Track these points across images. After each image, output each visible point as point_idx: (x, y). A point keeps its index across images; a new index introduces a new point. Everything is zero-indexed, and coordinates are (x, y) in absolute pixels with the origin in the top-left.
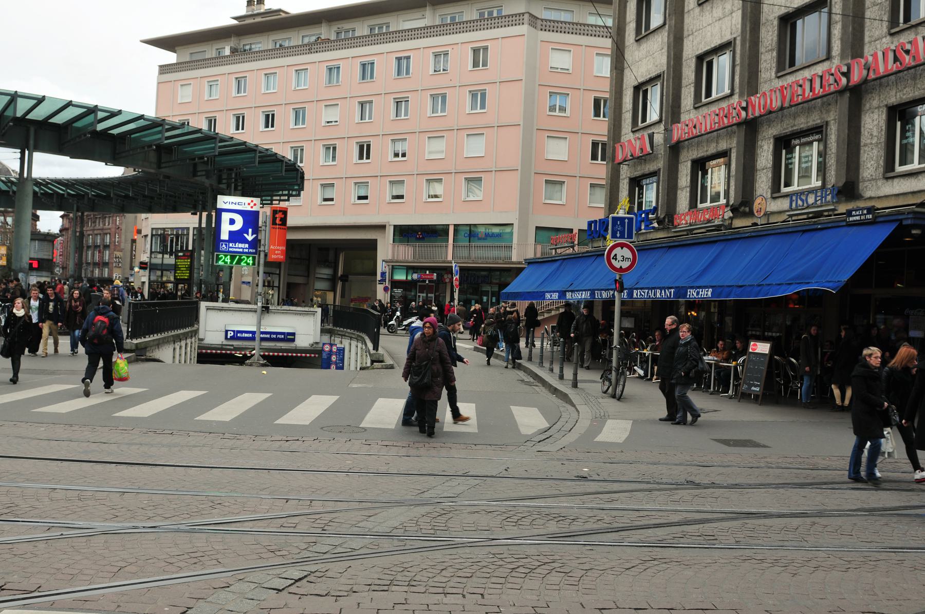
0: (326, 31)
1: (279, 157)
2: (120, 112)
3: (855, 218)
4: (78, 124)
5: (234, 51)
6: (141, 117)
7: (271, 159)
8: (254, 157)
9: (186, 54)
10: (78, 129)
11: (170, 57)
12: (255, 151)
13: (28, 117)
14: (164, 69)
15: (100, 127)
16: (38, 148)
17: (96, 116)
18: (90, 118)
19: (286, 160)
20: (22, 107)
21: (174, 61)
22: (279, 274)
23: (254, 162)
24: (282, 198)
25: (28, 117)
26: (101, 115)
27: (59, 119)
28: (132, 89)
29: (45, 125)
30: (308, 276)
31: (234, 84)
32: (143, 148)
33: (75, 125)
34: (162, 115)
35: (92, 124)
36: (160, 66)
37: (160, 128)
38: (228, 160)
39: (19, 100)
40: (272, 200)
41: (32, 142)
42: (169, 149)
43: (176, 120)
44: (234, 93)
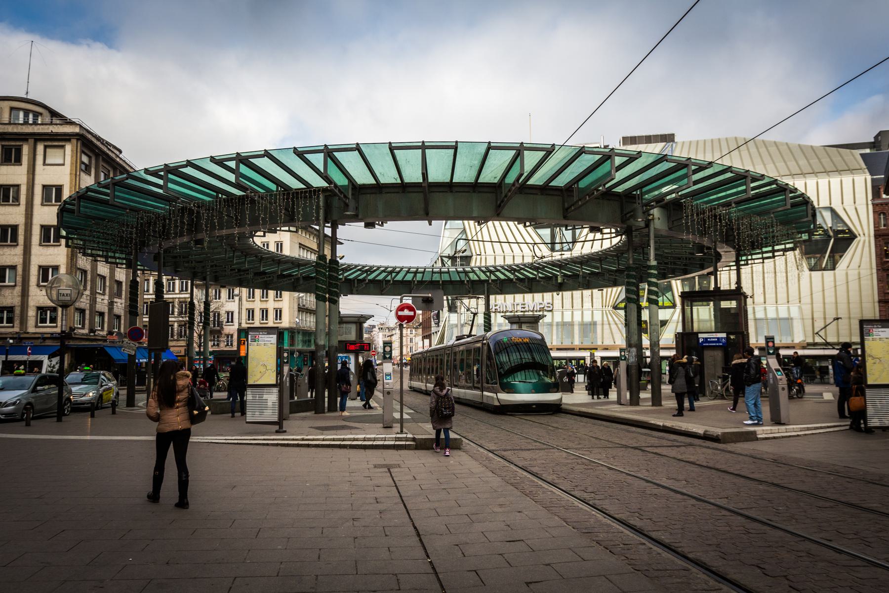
17: (613, 163)
18: (606, 167)
24: (765, 255)
25: (553, 184)
33: (582, 184)
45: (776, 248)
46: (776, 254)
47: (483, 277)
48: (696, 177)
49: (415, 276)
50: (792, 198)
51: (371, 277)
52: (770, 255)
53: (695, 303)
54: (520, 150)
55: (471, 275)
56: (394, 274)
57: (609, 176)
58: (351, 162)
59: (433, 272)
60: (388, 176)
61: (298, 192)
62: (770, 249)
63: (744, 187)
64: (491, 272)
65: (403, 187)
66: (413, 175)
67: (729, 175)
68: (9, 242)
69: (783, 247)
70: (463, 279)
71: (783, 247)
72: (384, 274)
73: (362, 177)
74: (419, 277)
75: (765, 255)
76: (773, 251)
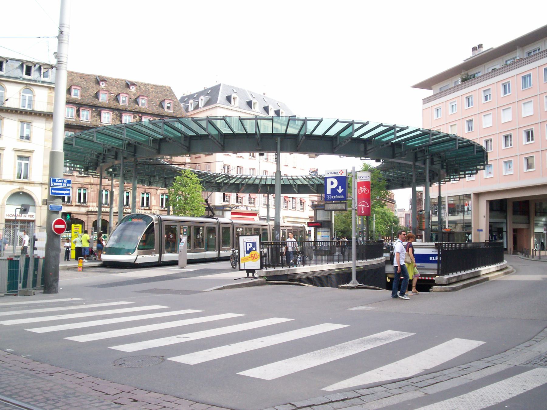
0: (519, 54)
1: (471, 142)
2: (368, 123)
3: (58, 184)
4: (343, 134)
5: (464, 80)
6: (448, 135)
7: (470, 145)
8: (455, 144)
9: (437, 89)
10: (342, 138)
11: (429, 93)
12: (455, 139)
13: (326, 134)
14: (426, 101)
15: (356, 135)
16: (283, 150)
17: (353, 128)
18: (349, 130)
19: (476, 144)
20: (310, 126)
21: (432, 94)
22: (506, 223)
23: (473, 152)
24: (461, 176)
25: (326, 134)
26: (356, 126)
27: (332, 133)
28: (410, 114)
29: (323, 137)
30: (529, 223)
31: (465, 101)
32: (383, 145)
33: (341, 135)
34: (427, 128)
35: (352, 133)
36: (423, 100)
37: (393, 131)
38: (435, 149)
39: (308, 122)
40: (450, 179)
41: (279, 147)
42: (398, 144)
43: (203, 89)
44: (466, 107)
45: (467, 172)
46: (467, 176)
47: (305, 183)
48: (398, 134)
49: (261, 181)
50: (459, 143)
51: (232, 182)
52: (463, 176)
53: (320, 229)
54: (305, 121)
55: (297, 181)
56: (247, 180)
57: (352, 133)
58: (220, 124)
59: (272, 179)
60: (238, 130)
61: (191, 137)
62: (463, 173)
63: (428, 139)
64: (309, 179)
65: (248, 135)
66: (251, 130)
67: (419, 132)
68: (22, 94)
69: (470, 172)
70: (292, 183)
71: (470, 172)
72: (240, 180)
73: (226, 131)
74: (263, 182)
75: (461, 176)
76: (465, 174)
